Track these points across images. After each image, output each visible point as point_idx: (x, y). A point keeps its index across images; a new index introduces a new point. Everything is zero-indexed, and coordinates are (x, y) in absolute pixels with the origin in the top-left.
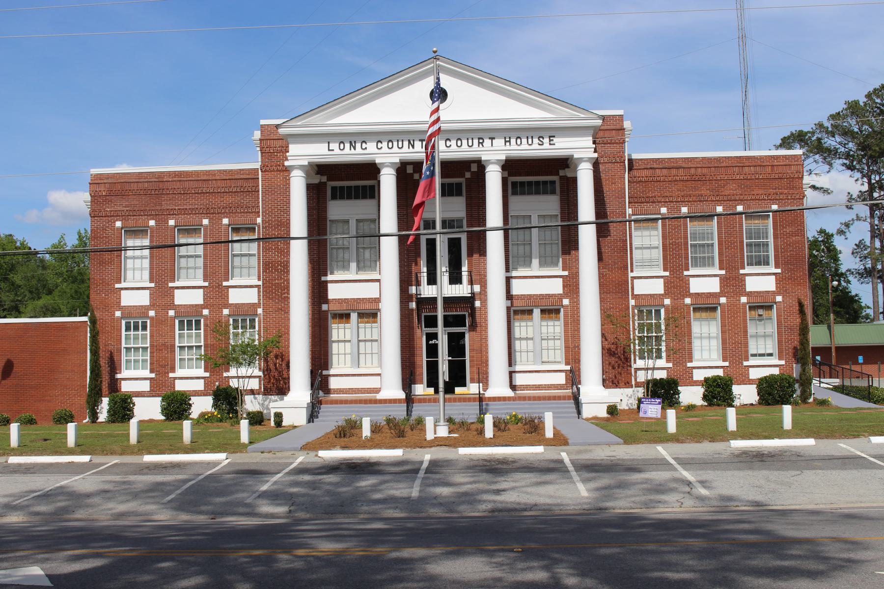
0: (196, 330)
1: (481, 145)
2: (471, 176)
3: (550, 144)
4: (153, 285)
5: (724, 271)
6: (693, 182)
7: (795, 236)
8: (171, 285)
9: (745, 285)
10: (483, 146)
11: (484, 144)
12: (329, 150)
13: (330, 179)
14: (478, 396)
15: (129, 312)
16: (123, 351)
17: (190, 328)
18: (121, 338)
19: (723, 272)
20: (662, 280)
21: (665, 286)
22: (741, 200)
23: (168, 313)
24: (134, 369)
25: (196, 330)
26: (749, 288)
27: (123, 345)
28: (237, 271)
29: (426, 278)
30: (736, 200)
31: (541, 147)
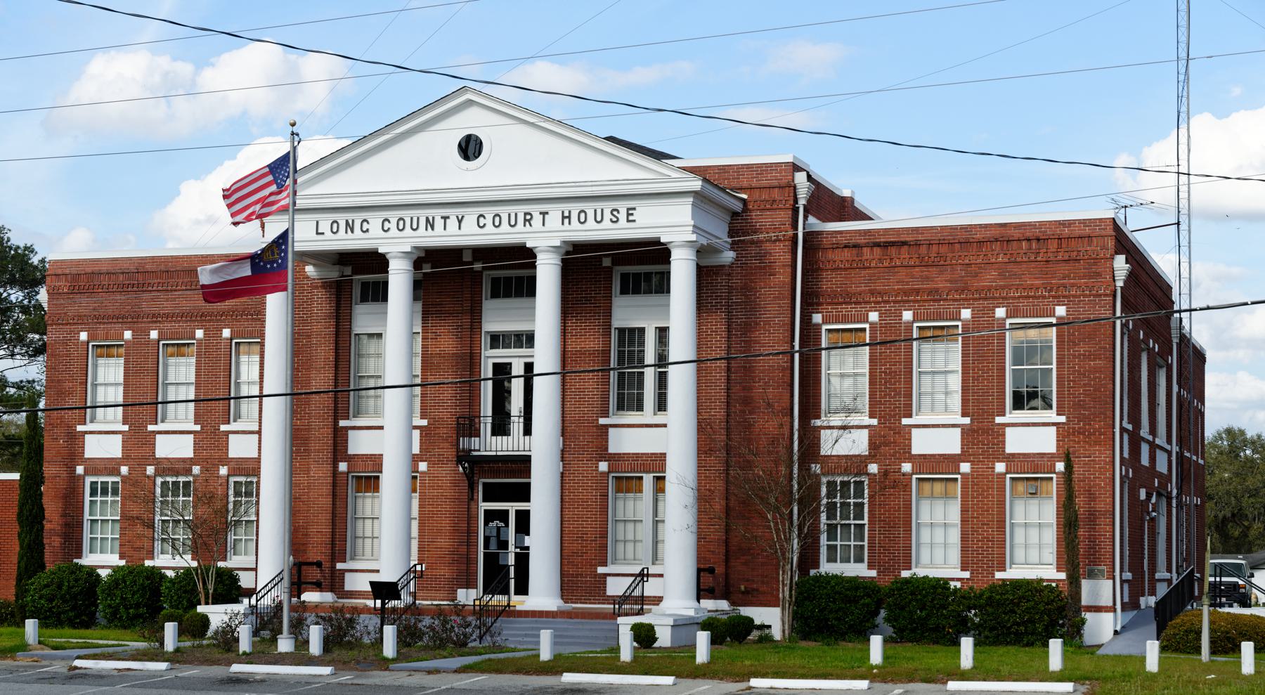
0: (184, 496)
1: (527, 223)
3: (628, 221)
4: (126, 428)
5: (969, 418)
7: (1095, 360)
8: (151, 428)
10: (531, 225)
11: (532, 222)
12: (317, 233)
13: (356, 271)
15: (98, 466)
16: (86, 526)
17: (176, 493)
20: (120, 437)
22: (1004, 298)
23: (597, 467)
24: (111, 553)
26: (1010, 448)
27: (87, 516)
28: (926, 400)
30: (994, 298)
31: (615, 226)
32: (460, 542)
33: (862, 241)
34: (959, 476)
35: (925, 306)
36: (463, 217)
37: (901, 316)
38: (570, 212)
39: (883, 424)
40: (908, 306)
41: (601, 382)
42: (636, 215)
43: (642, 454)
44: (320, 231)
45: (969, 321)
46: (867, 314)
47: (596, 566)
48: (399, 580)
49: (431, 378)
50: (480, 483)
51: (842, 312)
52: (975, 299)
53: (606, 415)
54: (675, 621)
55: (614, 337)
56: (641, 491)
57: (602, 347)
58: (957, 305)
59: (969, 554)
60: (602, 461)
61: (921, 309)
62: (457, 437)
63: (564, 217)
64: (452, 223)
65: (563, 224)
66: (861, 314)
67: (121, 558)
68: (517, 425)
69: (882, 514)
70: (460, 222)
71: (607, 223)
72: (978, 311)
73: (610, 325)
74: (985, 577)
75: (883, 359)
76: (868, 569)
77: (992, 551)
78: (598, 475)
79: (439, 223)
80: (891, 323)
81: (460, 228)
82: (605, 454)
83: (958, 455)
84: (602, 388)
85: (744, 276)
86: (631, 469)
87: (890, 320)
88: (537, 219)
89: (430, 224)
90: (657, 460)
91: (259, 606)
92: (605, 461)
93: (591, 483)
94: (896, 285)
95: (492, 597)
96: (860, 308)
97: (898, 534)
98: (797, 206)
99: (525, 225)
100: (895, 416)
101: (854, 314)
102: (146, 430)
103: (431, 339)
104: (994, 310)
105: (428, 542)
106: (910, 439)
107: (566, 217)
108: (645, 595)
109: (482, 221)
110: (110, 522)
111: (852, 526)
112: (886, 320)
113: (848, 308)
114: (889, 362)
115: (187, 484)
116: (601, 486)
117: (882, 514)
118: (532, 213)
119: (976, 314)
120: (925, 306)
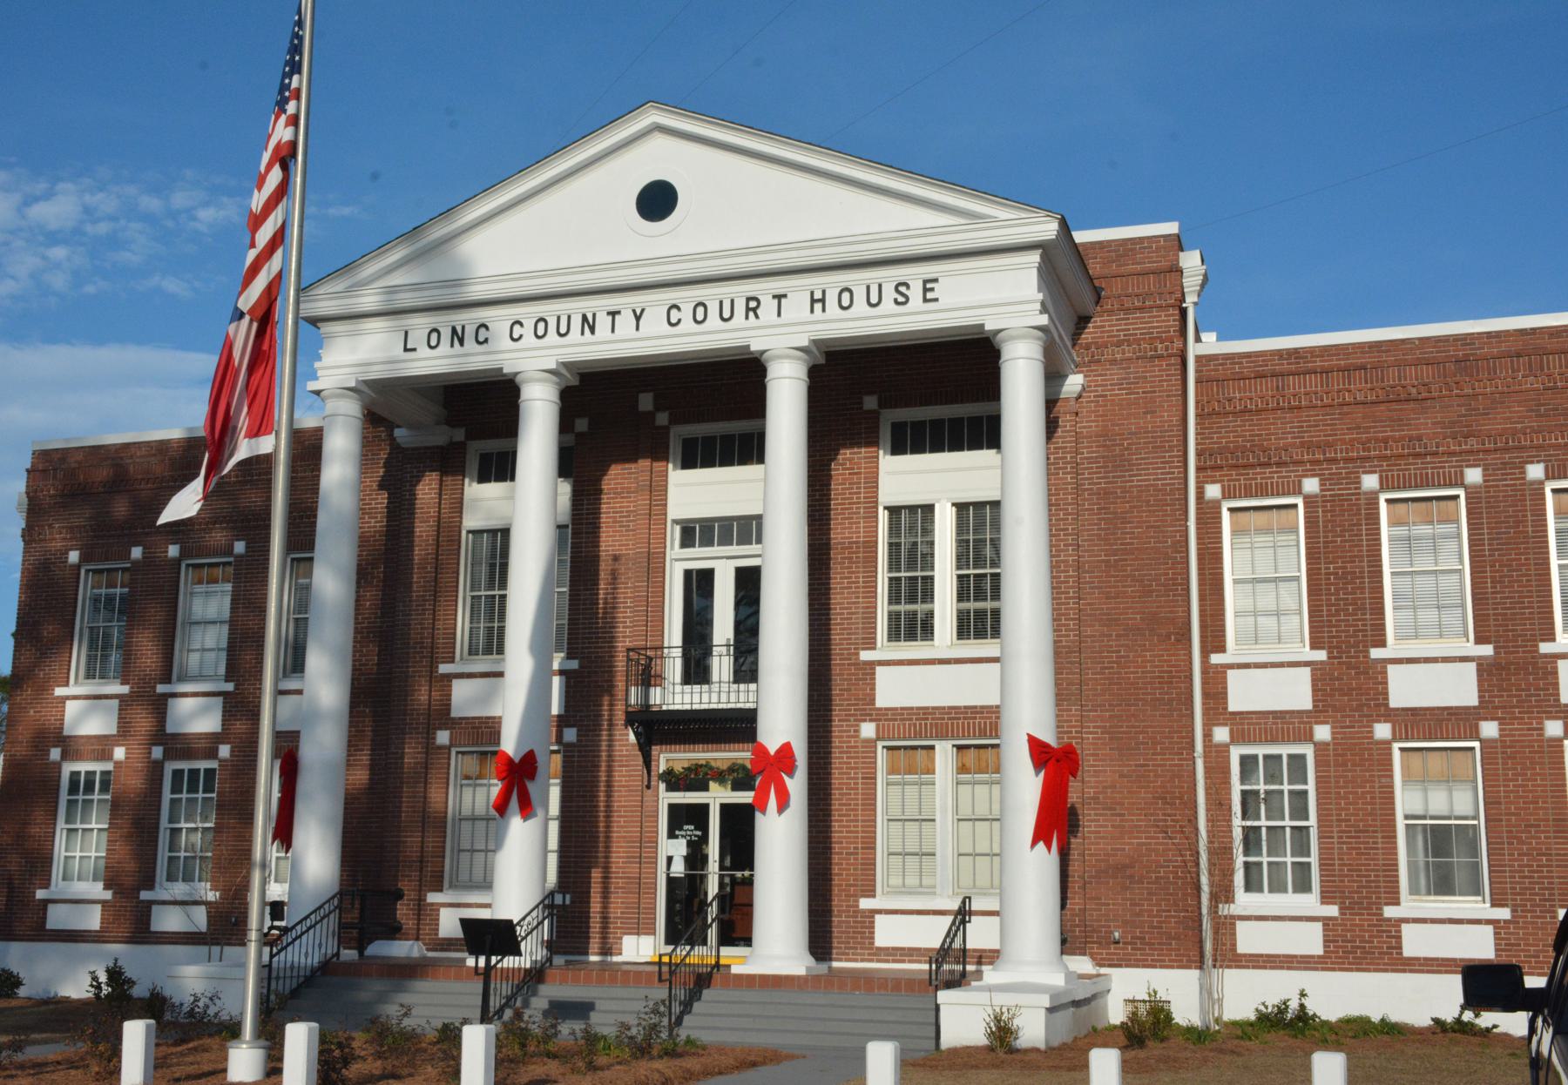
1: (751, 314)
2: (1537, 646)
3: (925, 300)
6: (1395, 406)
9: (1556, 685)
10: (757, 317)
11: (758, 312)
12: (406, 350)
14: (657, 968)
18: (159, 814)
19: (1487, 650)
20: (1307, 671)
21: (1315, 690)
22: (1539, 447)
23: (857, 731)
25: (204, 792)
29: (679, 663)
30: (1521, 448)
32: (628, 857)
33: (1286, 366)
34: (1476, 744)
35: (1400, 465)
36: (643, 310)
37: (1359, 483)
38: (824, 292)
39: (1335, 658)
40: (1370, 466)
41: (863, 592)
42: (939, 290)
43: (934, 708)
44: (409, 347)
45: (1480, 487)
46: (1300, 482)
47: (856, 897)
48: (524, 919)
49: (585, 595)
50: (661, 759)
51: (1256, 479)
52: (1487, 451)
53: (871, 644)
54: (1052, 998)
55: (883, 517)
56: (931, 770)
57: (864, 537)
58: (1457, 461)
59: (1505, 877)
60: (865, 721)
61: (1393, 470)
62: (627, 687)
63: (813, 301)
64: (626, 321)
65: (812, 311)
66: (1288, 482)
67: (106, 887)
68: (722, 665)
69: (1342, 809)
70: (638, 318)
71: (888, 305)
72: (1494, 470)
73: (877, 502)
74: (1538, 917)
75: (1331, 552)
76: (1322, 903)
77: (1375, 876)
78: (859, 744)
79: (603, 322)
80: (1342, 495)
81: (637, 329)
82: (870, 709)
83: (1474, 708)
84: (863, 603)
85: (1101, 416)
86: (915, 734)
87: (1339, 489)
88: (768, 305)
89: (589, 324)
90: (959, 719)
91: (275, 965)
92: (871, 720)
93: (842, 758)
94: (1347, 434)
95: (690, 950)
96: (1286, 472)
97: (1374, 843)
98: (1184, 305)
99: (747, 318)
100: (1356, 645)
101: (1277, 482)
102: (155, 692)
103: (586, 533)
104: (1523, 468)
105: (575, 857)
106: (1386, 683)
107: (818, 301)
108: (968, 947)
109: (675, 316)
110: (95, 831)
111: (1288, 830)
112: (1333, 490)
113: (1265, 473)
114: (1341, 557)
115: (210, 773)
116: (863, 763)
117: (1342, 809)
118: (759, 297)
119: (1490, 475)
120: (1400, 465)
